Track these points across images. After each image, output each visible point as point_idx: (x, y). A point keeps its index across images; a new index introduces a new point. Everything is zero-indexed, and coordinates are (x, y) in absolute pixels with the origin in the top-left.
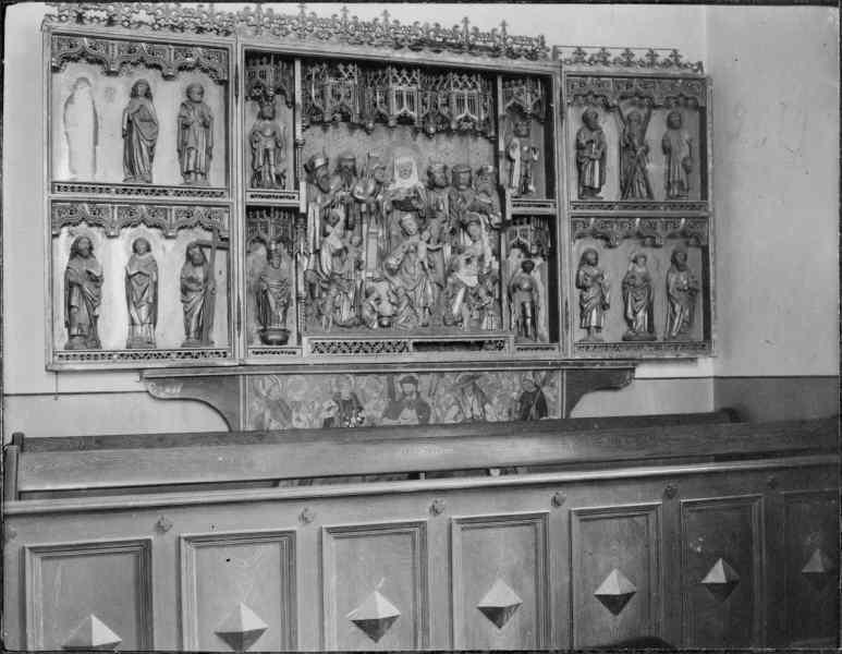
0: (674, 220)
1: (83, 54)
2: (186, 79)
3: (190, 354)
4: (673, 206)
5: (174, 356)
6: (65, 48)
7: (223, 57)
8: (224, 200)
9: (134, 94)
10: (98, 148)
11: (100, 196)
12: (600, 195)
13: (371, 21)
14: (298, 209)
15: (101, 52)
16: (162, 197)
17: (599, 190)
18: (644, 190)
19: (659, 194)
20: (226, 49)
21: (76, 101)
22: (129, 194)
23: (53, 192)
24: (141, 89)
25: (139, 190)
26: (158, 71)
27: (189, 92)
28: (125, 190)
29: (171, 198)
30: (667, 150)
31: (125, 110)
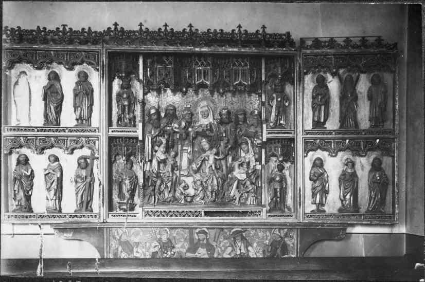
3: (76, 216)
14: (138, 137)
16: (62, 133)
21: (19, 83)
25: (50, 130)
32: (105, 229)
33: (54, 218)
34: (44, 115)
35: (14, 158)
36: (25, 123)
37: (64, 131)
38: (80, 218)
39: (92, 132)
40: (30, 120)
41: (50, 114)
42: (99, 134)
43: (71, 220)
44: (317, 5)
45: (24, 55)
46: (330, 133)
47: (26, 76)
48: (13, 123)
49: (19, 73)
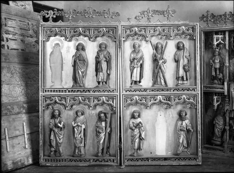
0: (154, 97)
1: (136, 34)
2: (100, 40)
3: (98, 160)
4: (178, 90)
5: (91, 161)
6: (128, 32)
7: (114, 31)
8: (114, 94)
9: (77, 49)
10: (63, 72)
11: (184, 92)
12: (141, 84)
13: (224, 13)
14: (224, 93)
15: (143, 32)
16: (87, 93)
17: (140, 82)
18: (163, 81)
19: (171, 82)
20: (116, 28)
21: (54, 53)
22: (74, 92)
23: (43, 92)
24: (80, 47)
25: (78, 91)
26: (151, 41)
27: (100, 46)
28: (72, 90)
29: (148, 92)
30: (177, 61)
31: (73, 56)
32: (115, 158)
33: (81, 161)
34: (73, 78)
35: (48, 113)
36: (58, 86)
37: (89, 91)
38: (101, 161)
39: (111, 92)
40: (62, 81)
41: (78, 77)
42: (197, 92)
43: (94, 163)
44: (4, 124)
45: (59, 31)
46: (145, 90)
47: (59, 47)
48: (49, 84)
49: (54, 45)
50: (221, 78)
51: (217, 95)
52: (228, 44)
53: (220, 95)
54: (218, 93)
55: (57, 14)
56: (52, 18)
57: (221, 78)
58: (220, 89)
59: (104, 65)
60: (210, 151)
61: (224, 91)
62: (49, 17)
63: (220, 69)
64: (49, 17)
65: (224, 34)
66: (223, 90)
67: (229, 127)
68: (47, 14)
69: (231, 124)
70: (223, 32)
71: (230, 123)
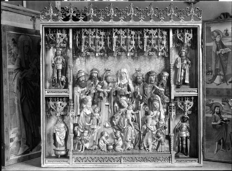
14: (68, 97)
50: (63, 81)
51: (61, 100)
52: (170, 42)
53: (64, 99)
54: (62, 98)
55: (77, 13)
56: (73, 16)
57: (63, 81)
58: (64, 93)
59: (54, 81)
60: (134, 165)
61: (69, 95)
62: (69, 16)
63: (62, 71)
64: (69, 16)
65: (68, 33)
66: (68, 94)
67: (73, 135)
68: (67, 13)
69: (76, 131)
70: (67, 30)
71: (75, 130)
